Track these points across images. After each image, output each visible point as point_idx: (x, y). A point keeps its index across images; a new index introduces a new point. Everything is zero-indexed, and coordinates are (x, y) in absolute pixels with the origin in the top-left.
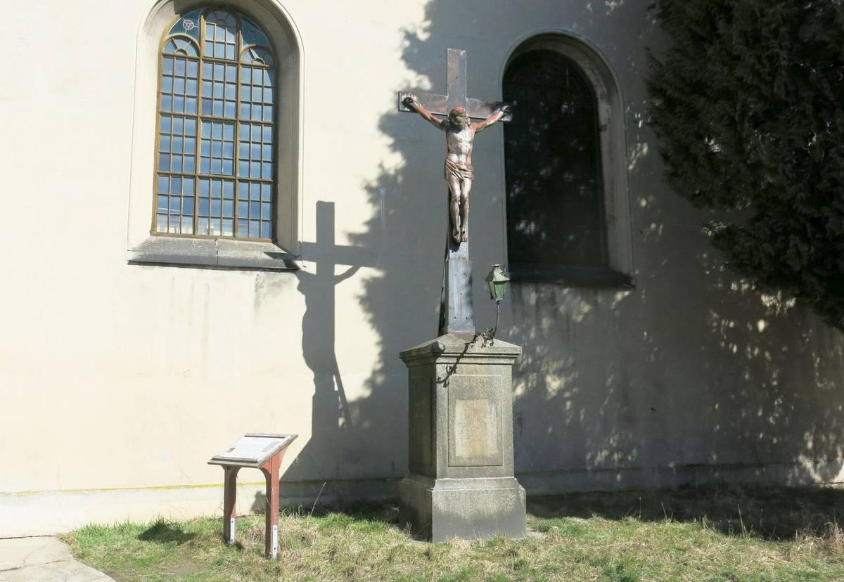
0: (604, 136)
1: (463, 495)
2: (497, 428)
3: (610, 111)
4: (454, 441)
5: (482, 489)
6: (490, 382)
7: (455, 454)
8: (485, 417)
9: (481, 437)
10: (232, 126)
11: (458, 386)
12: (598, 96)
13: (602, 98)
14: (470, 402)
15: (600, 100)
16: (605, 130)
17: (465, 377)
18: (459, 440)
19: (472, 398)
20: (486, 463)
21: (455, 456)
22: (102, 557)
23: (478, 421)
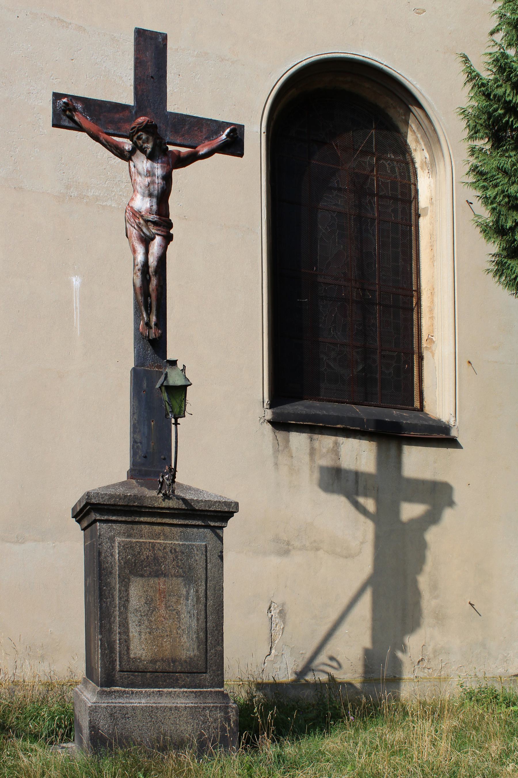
0: (423, 222)
1: (138, 712)
2: (198, 620)
3: (433, 186)
4: (128, 636)
5: (169, 705)
6: (187, 552)
7: (128, 653)
8: (177, 602)
9: (170, 631)
10: (174, 105)
11: (134, 555)
12: (417, 165)
13: (422, 168)
14: (152, 581)
15: (419, 172)
16: (426, 214)
17: (145, 543)
18: (136, 634)
19: (158, 574)
20: (179, 669)
21: (129, 658)
22: (250, 673)
23: (167, 607)
